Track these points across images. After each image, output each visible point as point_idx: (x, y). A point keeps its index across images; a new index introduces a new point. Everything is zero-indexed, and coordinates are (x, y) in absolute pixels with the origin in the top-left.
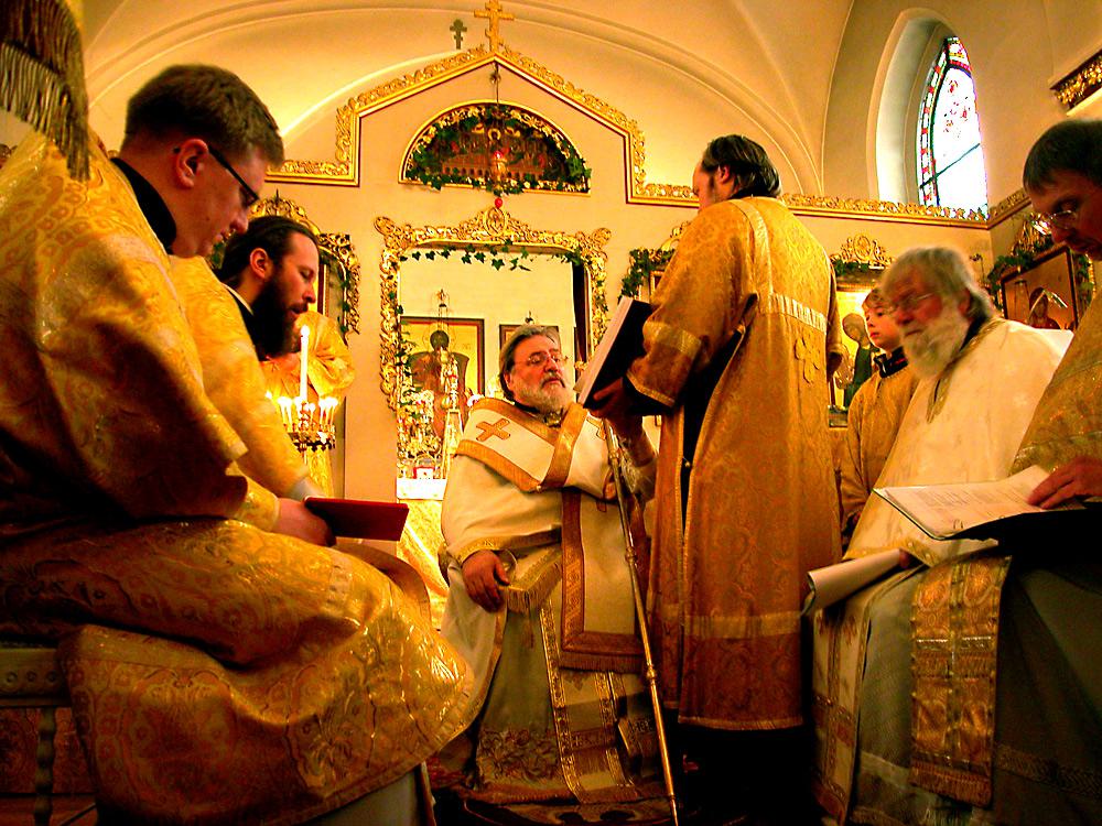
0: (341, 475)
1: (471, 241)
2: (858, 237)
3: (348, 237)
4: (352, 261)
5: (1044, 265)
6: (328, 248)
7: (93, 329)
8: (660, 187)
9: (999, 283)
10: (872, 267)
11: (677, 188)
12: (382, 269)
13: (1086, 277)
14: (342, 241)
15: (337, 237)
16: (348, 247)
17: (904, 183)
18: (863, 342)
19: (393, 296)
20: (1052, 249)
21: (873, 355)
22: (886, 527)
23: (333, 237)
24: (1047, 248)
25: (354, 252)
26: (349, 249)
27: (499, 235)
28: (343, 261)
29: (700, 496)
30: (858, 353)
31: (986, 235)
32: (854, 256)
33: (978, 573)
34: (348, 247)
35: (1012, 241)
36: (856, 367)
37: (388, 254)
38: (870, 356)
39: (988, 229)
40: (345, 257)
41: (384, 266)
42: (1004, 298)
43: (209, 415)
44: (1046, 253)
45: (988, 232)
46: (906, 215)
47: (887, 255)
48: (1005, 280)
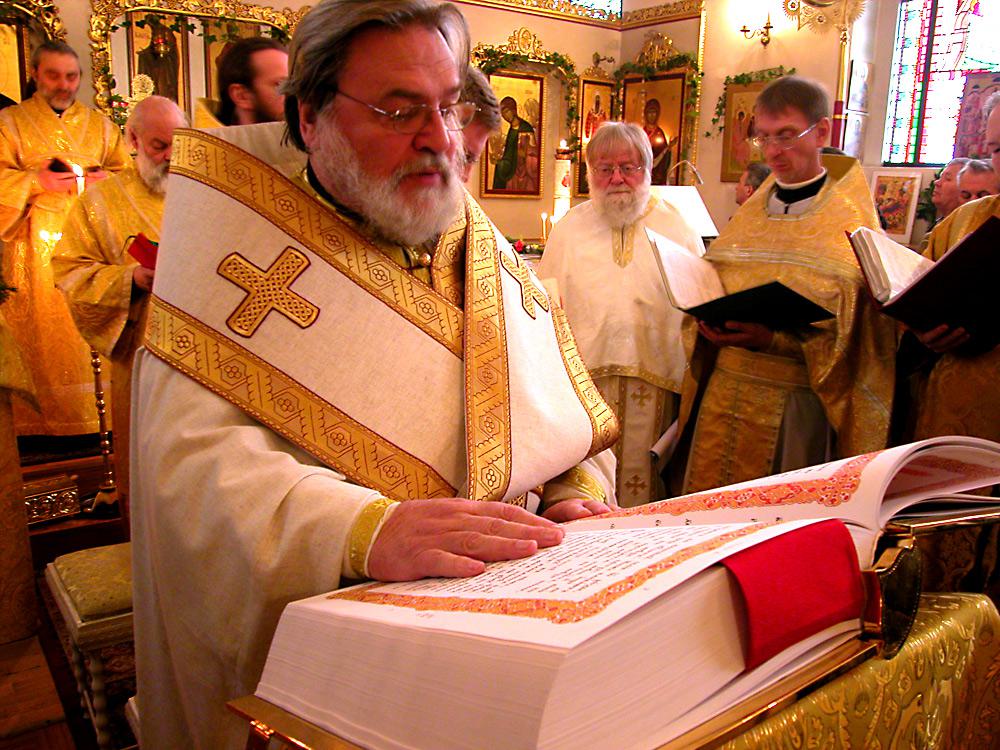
0: (404, 579)
1: (181, 11)
4: (57, 26)
5: (663, 81)
6: (30, 9)
7: (302, 541)
9: (622, 82)
12: (91, 37)
13: (694, 105)
17: (829, 685)
19: (106, 70)
20: (672, 72)
21: (520, 135)
24: (668, 70)
25: (58, 15)
26: (53, 12)
27: (210, 6)
28: (47, 25)
30: (509, 132)
31: (617, 35)
32: (518, 49)
35: (639, 50)
36: (506, 146)
37: (95, 20)
39: (620, 31)
40: (49, 21)
41: (93, 33)
42: (624, 95)
44: (666, 73)
45: (620, 33)
47: (543, 49)
48: (627, 81)
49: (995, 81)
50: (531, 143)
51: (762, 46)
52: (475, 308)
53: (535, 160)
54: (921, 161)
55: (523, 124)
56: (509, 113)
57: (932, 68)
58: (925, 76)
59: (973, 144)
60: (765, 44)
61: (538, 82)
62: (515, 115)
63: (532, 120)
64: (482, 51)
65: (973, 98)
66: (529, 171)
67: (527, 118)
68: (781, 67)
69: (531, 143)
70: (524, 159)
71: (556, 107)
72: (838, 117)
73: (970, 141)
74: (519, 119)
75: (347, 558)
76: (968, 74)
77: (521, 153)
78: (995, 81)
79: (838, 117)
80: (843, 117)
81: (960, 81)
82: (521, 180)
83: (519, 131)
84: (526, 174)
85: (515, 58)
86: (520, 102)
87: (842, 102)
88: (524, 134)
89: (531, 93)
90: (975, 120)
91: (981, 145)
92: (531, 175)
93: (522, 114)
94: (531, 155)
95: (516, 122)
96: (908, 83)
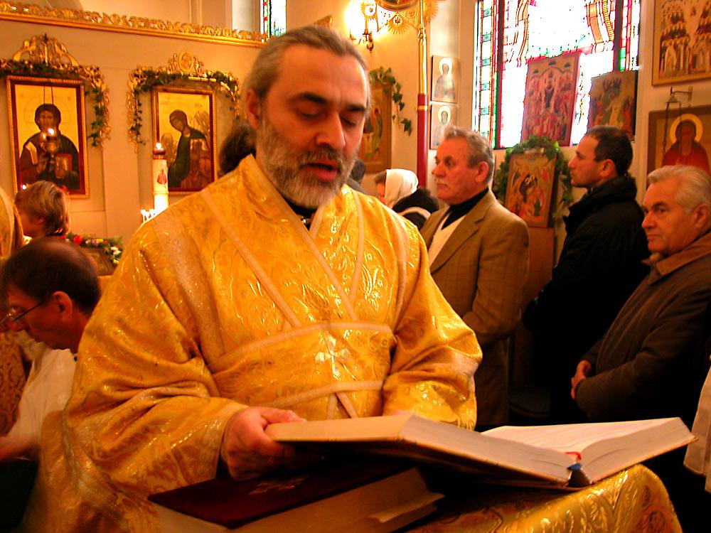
2: (182, 54)
3: (98, 69)
8: (140, 19)
10: (191, 78)
11: (154, 22)
14: (95, 71)
15: (91, 69)
16: (98, 76)
18: (185, 132)
22: (387, 352)
23: (89, 69)
29: (209, 285)
32: (178, 68)
33: (464, 411)
34: (98, 76)
36: (178, 151)
38: (189, 142)
43: (519, 513)
46: (210, 36)
47: (204, 68)
49: (550, 64)
50: (204, 148)
51: (369, 51)
52: (643, 204)
53: (209, 162)
54: (501, 144)
55: (195, 134)
56: (179, 124)
57: (505, 59)
58: (499, 64)
59: (536, 125)
60: (371, 49)
61: (208, 97)
62: (186, 125)
63: (204, 130)
64: (140, 71)
65: (534, 82)
66: (203, 171)
67: (198, 127)
68: (381, 68)
69: (204, 148)
70: (197, 162)
71: (228, 117)
72: (421, 108)
73: (533, 122)
74: (190, 128)
75: (311, 394)
76: (530, 61)
77: (194, 157)
78: (550, 64)
79: (421, 108)
80: (426, 108)
81: (524, 68)
82: (195, 179)
83: (190, 138)
84: (201, 174)
85: (174, 77)
86: (190, 114)
87: (423, 95)
88: (196, 141)
89: (201, 106)
90: (537, 103)
91: (542, 127)
92: (205, 175)
93: (193, 124)
94: (205, 158)
95: (187, 130)
96: (487, 74)
